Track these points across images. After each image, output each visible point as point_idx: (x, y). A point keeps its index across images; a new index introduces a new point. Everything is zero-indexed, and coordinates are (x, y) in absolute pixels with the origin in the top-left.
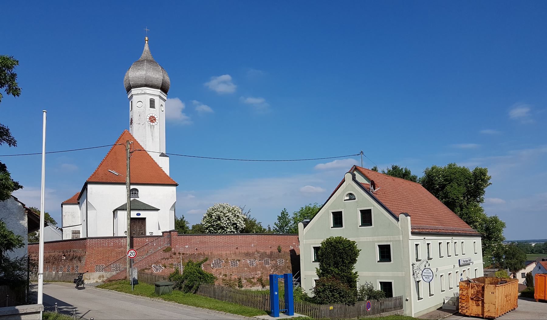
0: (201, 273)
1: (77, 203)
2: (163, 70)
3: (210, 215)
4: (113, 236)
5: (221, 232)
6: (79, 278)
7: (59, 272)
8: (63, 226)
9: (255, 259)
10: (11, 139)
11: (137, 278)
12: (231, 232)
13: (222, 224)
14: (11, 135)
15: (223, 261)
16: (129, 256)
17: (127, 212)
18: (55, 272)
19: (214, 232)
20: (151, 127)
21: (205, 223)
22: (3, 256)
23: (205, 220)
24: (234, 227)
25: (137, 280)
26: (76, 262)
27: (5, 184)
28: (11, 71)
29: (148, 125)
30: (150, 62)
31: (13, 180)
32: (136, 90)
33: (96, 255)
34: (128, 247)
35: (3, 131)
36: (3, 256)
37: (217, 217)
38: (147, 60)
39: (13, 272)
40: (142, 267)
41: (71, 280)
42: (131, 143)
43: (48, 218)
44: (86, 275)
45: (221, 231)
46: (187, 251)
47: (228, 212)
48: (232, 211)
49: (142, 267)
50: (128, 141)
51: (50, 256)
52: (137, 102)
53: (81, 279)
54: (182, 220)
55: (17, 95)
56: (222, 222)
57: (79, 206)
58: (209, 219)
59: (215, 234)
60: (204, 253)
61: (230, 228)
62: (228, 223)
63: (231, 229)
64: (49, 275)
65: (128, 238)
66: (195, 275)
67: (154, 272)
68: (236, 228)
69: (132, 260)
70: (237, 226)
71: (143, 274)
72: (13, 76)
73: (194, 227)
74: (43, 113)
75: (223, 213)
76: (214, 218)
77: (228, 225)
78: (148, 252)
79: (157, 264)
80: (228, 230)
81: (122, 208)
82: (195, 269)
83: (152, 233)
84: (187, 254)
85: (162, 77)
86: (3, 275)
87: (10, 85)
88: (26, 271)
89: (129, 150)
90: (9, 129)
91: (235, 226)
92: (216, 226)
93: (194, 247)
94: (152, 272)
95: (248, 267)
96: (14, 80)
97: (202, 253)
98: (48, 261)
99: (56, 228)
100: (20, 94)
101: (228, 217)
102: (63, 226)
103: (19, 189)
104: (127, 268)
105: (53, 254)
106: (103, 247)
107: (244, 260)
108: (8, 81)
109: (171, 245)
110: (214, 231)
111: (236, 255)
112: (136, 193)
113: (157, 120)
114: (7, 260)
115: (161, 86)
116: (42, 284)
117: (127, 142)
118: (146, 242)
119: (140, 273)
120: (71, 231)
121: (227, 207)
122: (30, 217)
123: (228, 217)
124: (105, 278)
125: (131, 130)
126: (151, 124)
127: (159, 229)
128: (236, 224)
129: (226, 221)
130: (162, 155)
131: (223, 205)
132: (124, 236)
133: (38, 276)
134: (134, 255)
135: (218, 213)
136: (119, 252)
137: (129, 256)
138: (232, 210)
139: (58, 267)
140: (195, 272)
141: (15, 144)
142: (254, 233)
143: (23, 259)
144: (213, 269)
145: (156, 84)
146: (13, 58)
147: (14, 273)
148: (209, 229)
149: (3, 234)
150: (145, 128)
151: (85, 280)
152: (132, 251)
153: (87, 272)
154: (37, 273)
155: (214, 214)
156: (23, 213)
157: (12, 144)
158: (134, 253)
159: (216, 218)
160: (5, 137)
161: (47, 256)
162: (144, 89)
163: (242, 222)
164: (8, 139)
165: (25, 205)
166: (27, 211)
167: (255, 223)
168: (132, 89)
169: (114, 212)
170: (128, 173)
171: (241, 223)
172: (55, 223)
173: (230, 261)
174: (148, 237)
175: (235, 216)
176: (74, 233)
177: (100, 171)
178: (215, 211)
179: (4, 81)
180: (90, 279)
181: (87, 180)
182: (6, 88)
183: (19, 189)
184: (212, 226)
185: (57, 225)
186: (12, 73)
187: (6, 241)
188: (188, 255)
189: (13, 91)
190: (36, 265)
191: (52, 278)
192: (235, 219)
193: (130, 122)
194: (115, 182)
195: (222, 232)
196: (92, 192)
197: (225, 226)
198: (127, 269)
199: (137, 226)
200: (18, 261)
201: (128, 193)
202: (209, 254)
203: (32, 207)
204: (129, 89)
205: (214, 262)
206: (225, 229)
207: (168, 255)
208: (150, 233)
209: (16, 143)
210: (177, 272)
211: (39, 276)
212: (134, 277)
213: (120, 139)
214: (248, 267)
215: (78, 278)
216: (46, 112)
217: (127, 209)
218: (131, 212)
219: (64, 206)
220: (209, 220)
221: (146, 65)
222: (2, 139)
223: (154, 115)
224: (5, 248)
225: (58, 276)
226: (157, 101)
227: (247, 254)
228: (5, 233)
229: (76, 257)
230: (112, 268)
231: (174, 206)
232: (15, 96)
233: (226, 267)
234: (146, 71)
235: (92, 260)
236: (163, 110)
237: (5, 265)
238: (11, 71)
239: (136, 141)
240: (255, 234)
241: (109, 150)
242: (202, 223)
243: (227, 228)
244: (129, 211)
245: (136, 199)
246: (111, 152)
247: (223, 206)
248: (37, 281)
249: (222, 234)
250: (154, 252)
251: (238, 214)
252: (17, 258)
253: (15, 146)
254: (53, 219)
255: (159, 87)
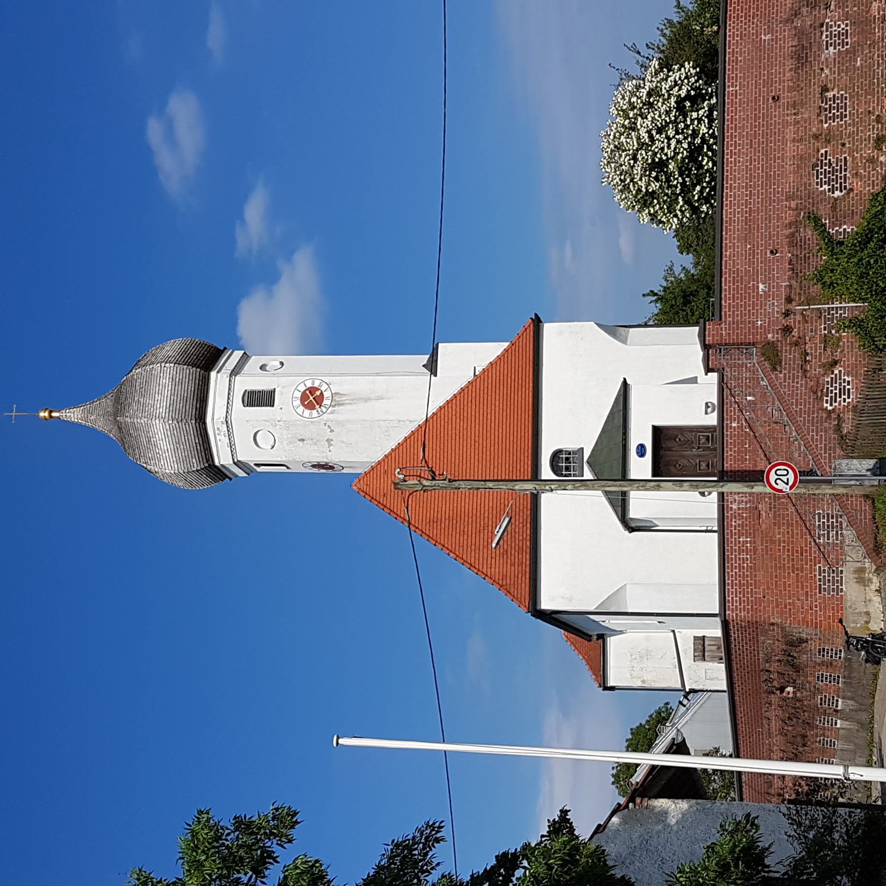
0: (864, 239)
1: (601, 641)
2: (142, 362)
3: (646, 200)
4: (716, 534)
5: (710, 158)
6: (863, 648)
7: (839, 708)
8: (679, 686)
9: (822, 25)
10: (422, 837)
11: (871, 463)
12: (711, 120)
13: (678, 153)
14: (410, 837)
15: (823, 151)
16: (791, 488)
17: (631, 492)
18: (839, 721)
19: (707, 183)
20: (339, 405)
21: (676, 216)
22: (786, 877)
23: (664, 219)
24: (692, 106)
25: (880, 459)
26: (804, 653)
27: (562, 859)
28: (227, 832)
29: (331, 413)
30: (119, 407)
31: (542, 836)
32: (218, 451)
33: (780, 591)
34: (758, 488)
35: (399, 856)
36: (784, 874)
37: (654, 174)
38: (116, 415)
39: (836, 849)
40: (830, 443)
41: (867, 672)
42: (401, 477)
43: (649, 730)
44: (852, 625)
45: (707, 156)
46: (779, 287)
47: (633, 133)
48: (629, 118)
49: (830, 443)
50: (395, 484)
51: (782, 733)
52: (255, 446)
53: (867, 642)
54: (661, 299)
55: (293, 816)
56: (670, 154)
57: (611, 636)
58: (659, 203)
59: (719, 179)
60: (790, 224)
61: (696, 122)
62: (677, 133)
63: (700, 120)
64: (847, 739)
65: (724, 489)
66: (872, 261)
67: (850, 400)
68: (696, 98)
69: (806, 475)
70: (688, 97)
71: (856, 439)
72: (243, 825)
73: (685, 248)
74: (342, 745)
75: (637, 150)
76: (658, 184)
77: (683, 133)
78: (776, 423)
79: (822, 391)
80: (703, 129)
81: (620, 505)
82: (848, 262)
83: (707, 404)
84: (790, 286)
85: (167, 365)
86: (845, 880)
87: (265, 833)
88: (834, 812)
89: (425, 483)
90: (393, 841)
91: (688, 104)
92: (688, 176)
93: (765, 261)
94: (850, 407)
95: (852, 53)
96: (253, 822)
97: (788, 232)
98: (799, 739)
99: (684, 706)
100: (289, 808)
101: (654, 132)
102: (679, 686)
103: (570, 819)
104: (831, 492)
105: (775, 725)
106: (753, 569)
107: (822, 69)
108: (256, 838)
109: (754, 344)
110: (705, 184)
111: (802, 104)
112: (567, 459)
113: (313, 383)
114: (798, 865)
115: (198, 370)
116: (882, 770)
117: (400, 489)
118: (741, 427)
119: (852, 450)
120: (697, 663)
121: (618, 134)
122: (656, 790)
123: (654, 132)
124: (867, 565)
125: (350, 467)
126: (326, 402)
127: (694, 380)
128: (680, 101)
129: (669, 138)
130: (432, 367)
131: (609, 150)
132: (719, 501)
133: (852, 781)
134: (785, 472)
135: (638, 170)
136: (775, 519)
137: (788, 487)
138: (627, 117)
139: (821, 710)
140: (860, 260)
141: (437, 825)
142: (717, 32)
143: (792, 819)
144: (851, 190)
145: (192, 387)
146: (191, 824)
147: (839, 847)
148: (698, 201)
149: (716, 871)
150: (337, 422)
151: (869, 629)
152: (773, 477)
153: (841, 621)
154: (843, 785)
155: (643, 184)
156: (645, 812)
157: (436, 834)
158: (778, 472)
159: (657, 179)
160: (416, 852)
161: (784, 742)
162: (213, 425)
163: (672, 78)
164: (421, 845)
165: (619, 804)
166: (638, 800)
167: (679, 23)
168: (217, 463)
169: (632, 530)
170: (503, 486)
171: (675, 81)
172: (667, 710)
173: (826, 126)
174: (721, 418)
175: (651, 105)
176: (704, 655)
177: (493, 570)
178: (632, 180)
179: (257, 850)
180: (868, 613)
181: (526, 610)
182: (274, 845)
183: (570, 819)
184: (686, 190)
185: (674, 705)
186: (232, 828)
187: (737, 866)
188: (793, 282)
189: (284, 826)
190: (815, 784)
191: (858, 730)
192: (663, 103)
193: (323, 471)
194: (528, 526)
195: (710, 154)
196: (563, 598)
197: (689, 143)
198: (835, 492)
199: (683, 457)
200: (799, 834)
201: (570, 487)
202: (793, 204)
203: (613, 776)
204: (217, 473)
205: (826, 187)
206: (698, 141)
207: (789, 355)
208: (706, 413)
209: (434, 824)
210: (856, 324)
211: (852, 777)
212: (868, 470)
213: (385, 507)
214: (852, 53)
215: (863, 653)
216: (338, 738)
217: (625, 489)
218: (632, 478)
219: (611, 683)
220: (664, 202)
221: (134, 418)
222: (424, 860)
223: (299, 395)
224: (760, 868)
225: (853, 712)
226: (249, 381)
227: (799, 58)
228: (713, 865)
229: (789, 655)
230: (831, 541)
231: (613, 330)
232: (297, 822)
233: (846, 141)
234: (151, 416)
235: (799, 603)
236: (278, 364)
237: (814, 871)
238: (230, 831)
239: (390, 454)
240: (722, 27)
241: (430, 545)
242: (674, 227)
243: (695, 134)
244: (630, 485)
245: (586, 458)
246: (429, 536)
247: (612, 151)
248: (868, 784)
249: (719, 154)
250: (777, 403)
251: (644, 92)
252: (789, 836)
253: (442, 825)
254: (651, 716)
255: (204, 377)
